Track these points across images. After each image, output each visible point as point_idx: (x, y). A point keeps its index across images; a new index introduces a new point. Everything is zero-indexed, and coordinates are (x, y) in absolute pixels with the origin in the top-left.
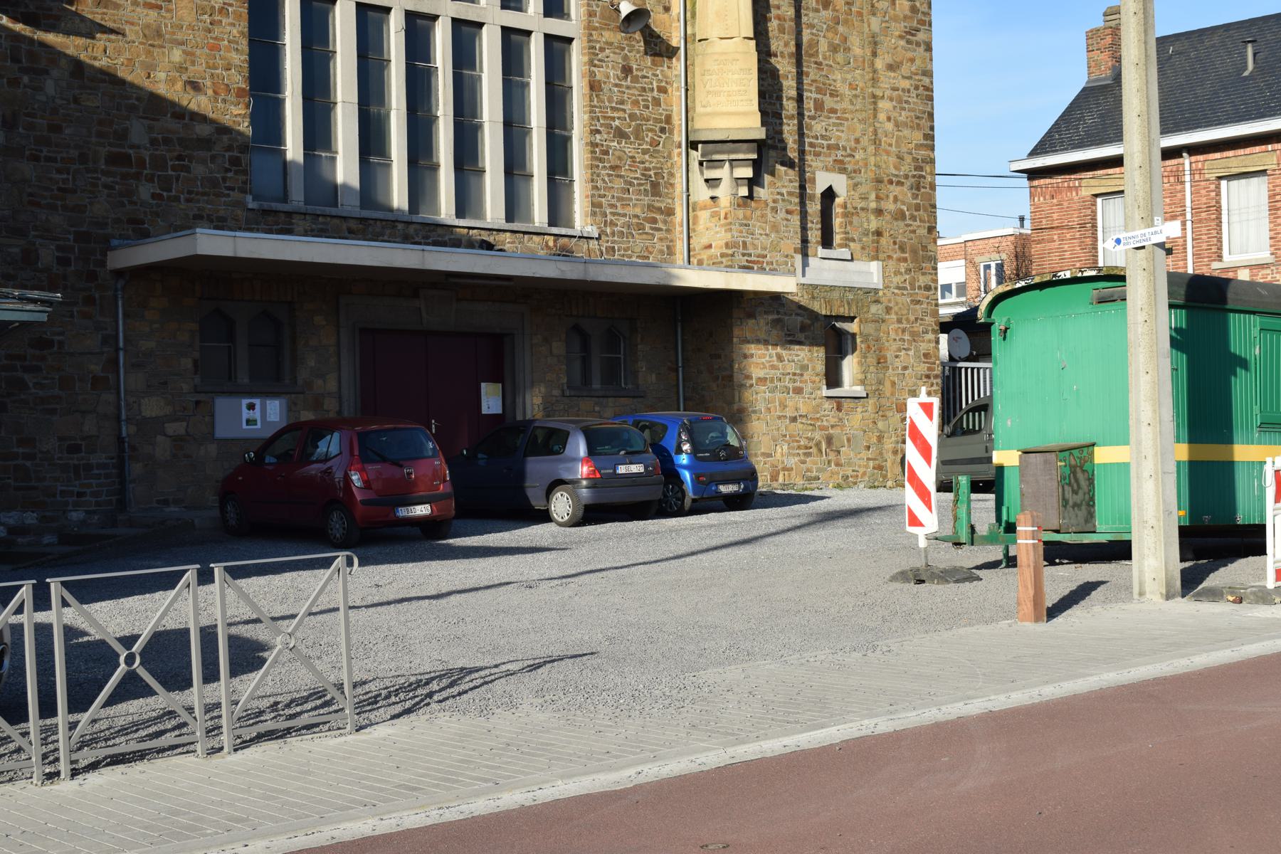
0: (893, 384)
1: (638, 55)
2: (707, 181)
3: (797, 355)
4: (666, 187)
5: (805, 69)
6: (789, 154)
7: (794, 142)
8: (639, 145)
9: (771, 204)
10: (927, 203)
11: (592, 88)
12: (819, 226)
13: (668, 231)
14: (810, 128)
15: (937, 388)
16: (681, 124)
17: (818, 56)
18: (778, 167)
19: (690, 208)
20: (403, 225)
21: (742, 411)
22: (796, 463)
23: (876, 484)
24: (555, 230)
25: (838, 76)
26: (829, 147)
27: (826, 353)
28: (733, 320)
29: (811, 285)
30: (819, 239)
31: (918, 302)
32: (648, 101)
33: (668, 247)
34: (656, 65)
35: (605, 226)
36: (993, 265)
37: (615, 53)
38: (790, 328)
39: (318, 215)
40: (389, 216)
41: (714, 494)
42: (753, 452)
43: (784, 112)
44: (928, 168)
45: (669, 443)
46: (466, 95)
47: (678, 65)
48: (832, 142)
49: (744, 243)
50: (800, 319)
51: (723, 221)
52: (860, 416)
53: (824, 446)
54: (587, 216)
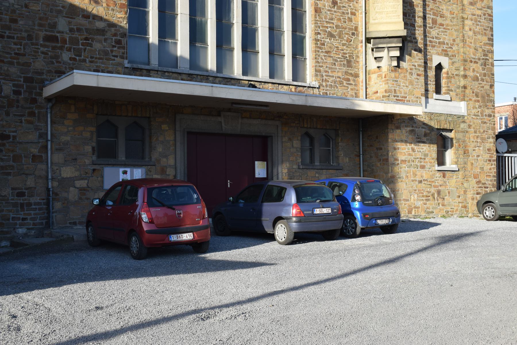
0: (472, 164)
2: (375, 58)
3: (422, 149)
4: (355, 63)
5: (427, 3)
6: (419, 45)
7: (422, 39)
8: (341, 41)
9: (409, 71)
10: (489, 73)
11: (316, 11)
12: (434, 83)
13: (355, 85)
14: (430, 33)
15: (495, 166)
16: (362, 31)
18: (413, 52)
19: (367, 73)
20: (212, 78)
21: (393, 177)
22: (421, 204)
23: (463, 215)
24: (295, 83)
25: (444, 7)
26: (439, 43)
27: (438, 148)
28: (389, 130)
29: (430, 113)
30: (434, 90)
31: (485, 123)
32: (345, 19)
33: (356, 93)
36: (503, 118)
38: (418, 135)
39: (165, 72)
40: (205, 73)
41: (374, 225)
42: (399, 199)
43: (416, 24)
44: (490, 55)
45: (348, 195)
46: (249, 13)
48: (441, 40)
49: (395, 90)
50: (424, 130)
51: (384, 79)
52: (455, 180)
53: (436, 196)
54: (313, 77)
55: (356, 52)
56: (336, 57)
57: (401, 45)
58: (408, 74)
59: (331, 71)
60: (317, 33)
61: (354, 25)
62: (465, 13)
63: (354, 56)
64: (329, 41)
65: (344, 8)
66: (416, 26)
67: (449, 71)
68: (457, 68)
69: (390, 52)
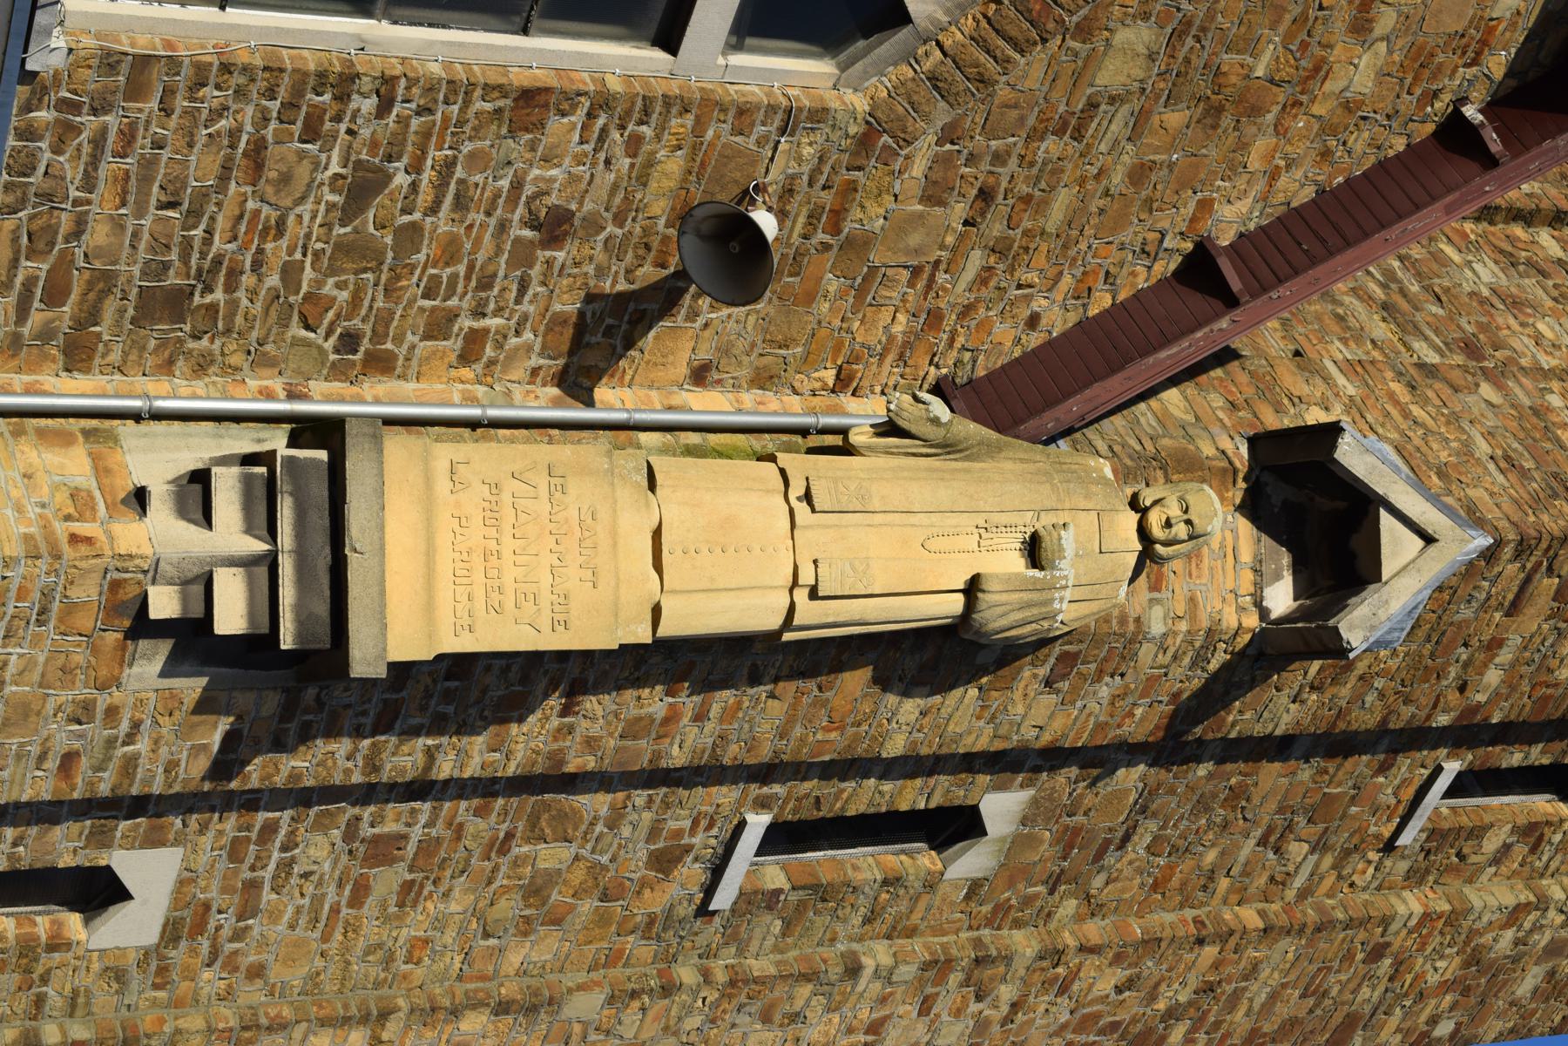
1: (590, 269)
4: (163, 344)
7: (295, 776)
8: (317, 255)
14: (320, 826)
16: (362, 401)
17: (528, 841)
18: (224, 724)
19: (94, 423)
26: (253, 886)
34: (549, 329)
35: (66, 106)
37: (615, 187)
43: (394, 739)
47: (543, 403)
48: (267, 896)
51: (61, 529)
55: (236, 359)
56: (220, 218)
57: (283, 647)
58: (82, 692)
59: (127, 172)
60: (393, 88)
61: (405, 346)
62: (408, 1027)
63: (212, 341)
64: (329, 173)
65: (514, 287)
66: (383, 738)
67: (70, 954)
68: (81, 1000)
69: (239, 571)
